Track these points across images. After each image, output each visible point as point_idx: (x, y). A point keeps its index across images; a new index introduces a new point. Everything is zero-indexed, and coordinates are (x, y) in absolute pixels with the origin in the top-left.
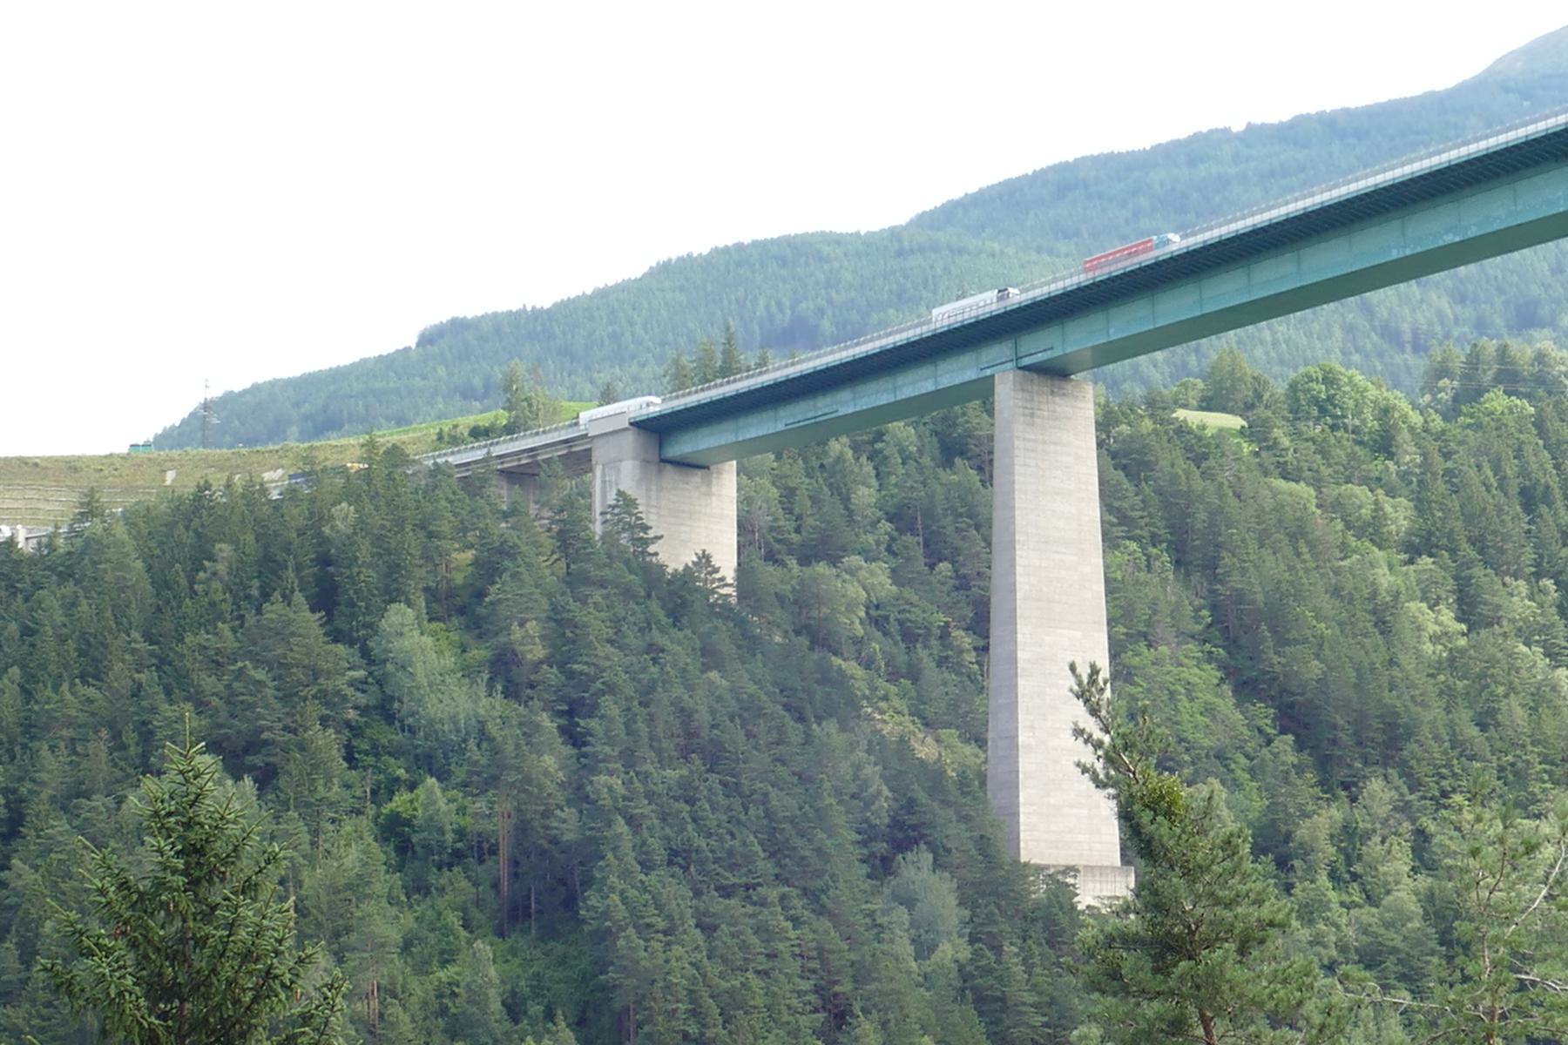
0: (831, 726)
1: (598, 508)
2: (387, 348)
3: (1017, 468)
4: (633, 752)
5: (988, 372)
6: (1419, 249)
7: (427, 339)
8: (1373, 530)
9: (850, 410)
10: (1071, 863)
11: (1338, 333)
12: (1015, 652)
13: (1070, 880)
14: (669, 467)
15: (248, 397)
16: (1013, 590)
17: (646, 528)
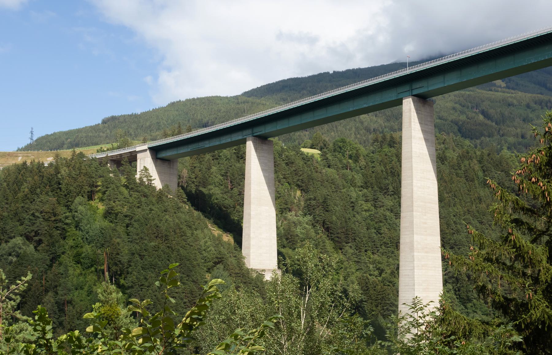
0: (199, 232)
1: (138, 170)
2: (93, 124)
3: (252, 163)
4: (79, 223)
5: (245, 137)
6: (357, 108)
7: (104, 122)
8: (352, 183)
9: (208, 146)
10: (264, 268)
11: (354, 129)
12: (250, 212)
13: (263, 273)
14: (159, 160)
15: (52, 137)
16: (250, 196)
17: (151, 177)
